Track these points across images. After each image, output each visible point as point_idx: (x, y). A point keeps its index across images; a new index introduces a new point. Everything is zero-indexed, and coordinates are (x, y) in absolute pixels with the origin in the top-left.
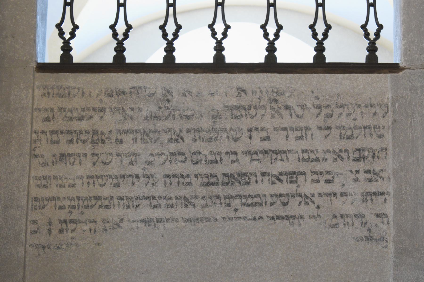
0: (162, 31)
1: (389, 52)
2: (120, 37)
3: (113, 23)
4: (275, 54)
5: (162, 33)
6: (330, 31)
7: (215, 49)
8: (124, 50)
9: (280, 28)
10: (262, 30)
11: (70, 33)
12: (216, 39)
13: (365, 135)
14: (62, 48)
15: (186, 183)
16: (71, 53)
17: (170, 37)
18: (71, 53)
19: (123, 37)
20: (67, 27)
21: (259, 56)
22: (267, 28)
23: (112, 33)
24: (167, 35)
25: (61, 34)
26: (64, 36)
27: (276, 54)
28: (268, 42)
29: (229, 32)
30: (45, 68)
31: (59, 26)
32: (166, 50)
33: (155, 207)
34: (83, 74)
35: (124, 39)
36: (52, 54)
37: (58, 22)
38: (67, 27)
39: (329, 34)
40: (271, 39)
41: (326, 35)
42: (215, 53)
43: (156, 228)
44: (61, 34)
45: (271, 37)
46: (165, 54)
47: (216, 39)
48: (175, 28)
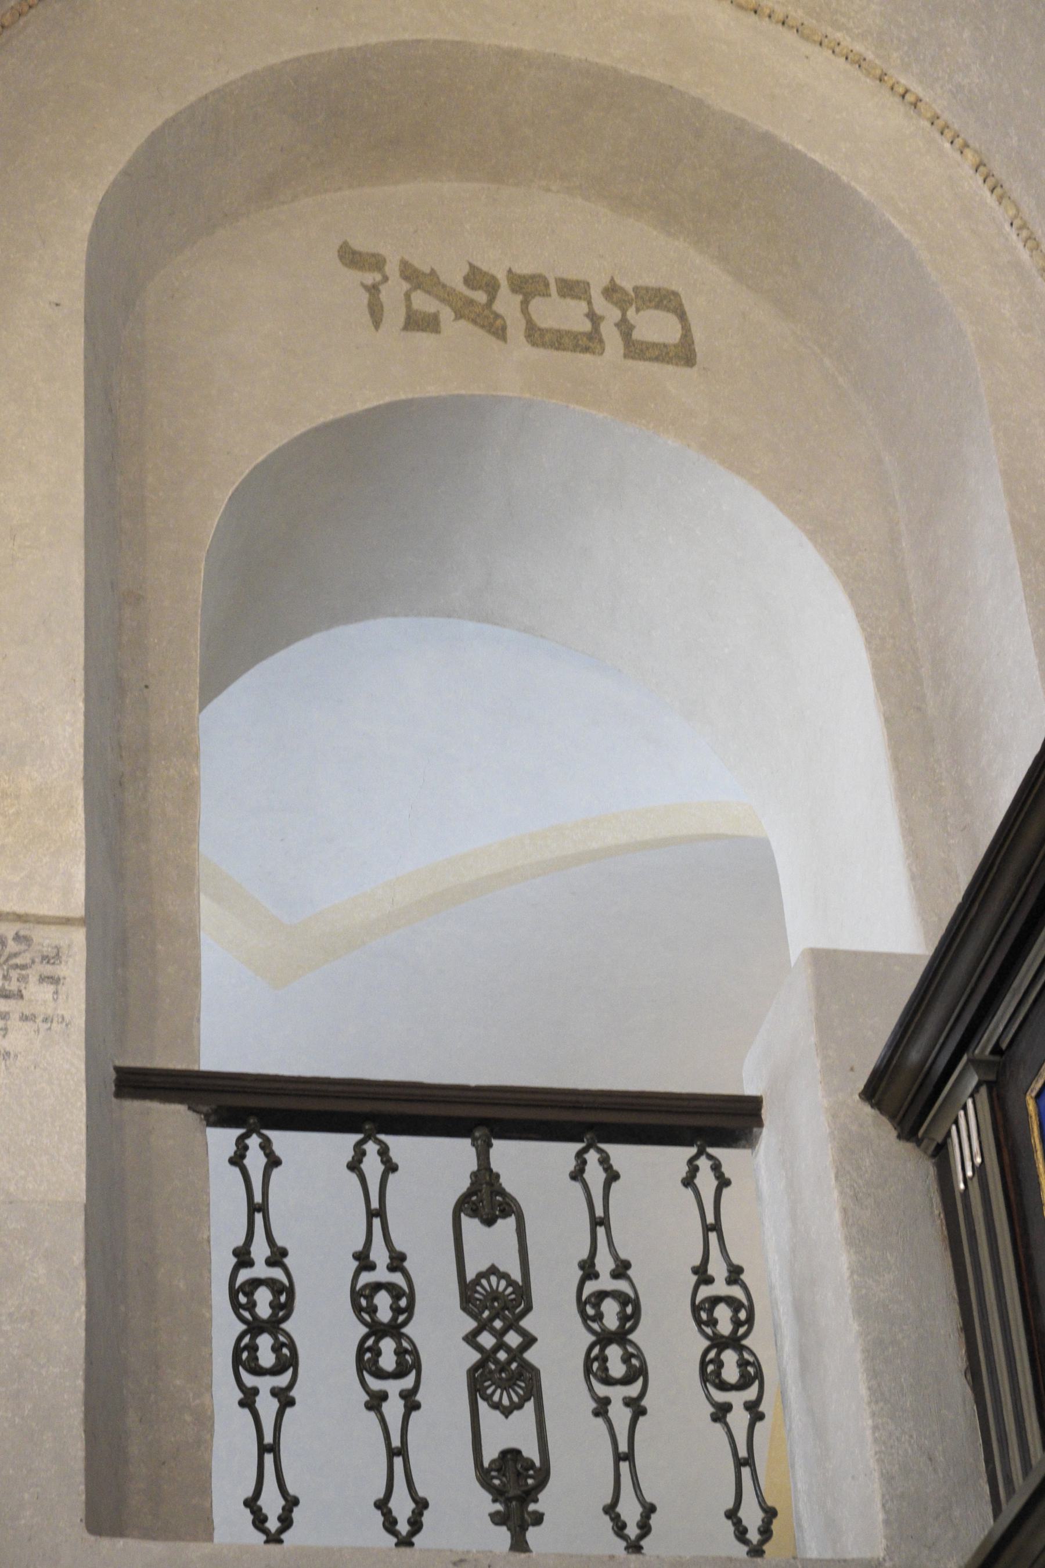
6: (426, 1513)
29: (427, 1518)
40: (633, 1537)
47: (265, 1531)
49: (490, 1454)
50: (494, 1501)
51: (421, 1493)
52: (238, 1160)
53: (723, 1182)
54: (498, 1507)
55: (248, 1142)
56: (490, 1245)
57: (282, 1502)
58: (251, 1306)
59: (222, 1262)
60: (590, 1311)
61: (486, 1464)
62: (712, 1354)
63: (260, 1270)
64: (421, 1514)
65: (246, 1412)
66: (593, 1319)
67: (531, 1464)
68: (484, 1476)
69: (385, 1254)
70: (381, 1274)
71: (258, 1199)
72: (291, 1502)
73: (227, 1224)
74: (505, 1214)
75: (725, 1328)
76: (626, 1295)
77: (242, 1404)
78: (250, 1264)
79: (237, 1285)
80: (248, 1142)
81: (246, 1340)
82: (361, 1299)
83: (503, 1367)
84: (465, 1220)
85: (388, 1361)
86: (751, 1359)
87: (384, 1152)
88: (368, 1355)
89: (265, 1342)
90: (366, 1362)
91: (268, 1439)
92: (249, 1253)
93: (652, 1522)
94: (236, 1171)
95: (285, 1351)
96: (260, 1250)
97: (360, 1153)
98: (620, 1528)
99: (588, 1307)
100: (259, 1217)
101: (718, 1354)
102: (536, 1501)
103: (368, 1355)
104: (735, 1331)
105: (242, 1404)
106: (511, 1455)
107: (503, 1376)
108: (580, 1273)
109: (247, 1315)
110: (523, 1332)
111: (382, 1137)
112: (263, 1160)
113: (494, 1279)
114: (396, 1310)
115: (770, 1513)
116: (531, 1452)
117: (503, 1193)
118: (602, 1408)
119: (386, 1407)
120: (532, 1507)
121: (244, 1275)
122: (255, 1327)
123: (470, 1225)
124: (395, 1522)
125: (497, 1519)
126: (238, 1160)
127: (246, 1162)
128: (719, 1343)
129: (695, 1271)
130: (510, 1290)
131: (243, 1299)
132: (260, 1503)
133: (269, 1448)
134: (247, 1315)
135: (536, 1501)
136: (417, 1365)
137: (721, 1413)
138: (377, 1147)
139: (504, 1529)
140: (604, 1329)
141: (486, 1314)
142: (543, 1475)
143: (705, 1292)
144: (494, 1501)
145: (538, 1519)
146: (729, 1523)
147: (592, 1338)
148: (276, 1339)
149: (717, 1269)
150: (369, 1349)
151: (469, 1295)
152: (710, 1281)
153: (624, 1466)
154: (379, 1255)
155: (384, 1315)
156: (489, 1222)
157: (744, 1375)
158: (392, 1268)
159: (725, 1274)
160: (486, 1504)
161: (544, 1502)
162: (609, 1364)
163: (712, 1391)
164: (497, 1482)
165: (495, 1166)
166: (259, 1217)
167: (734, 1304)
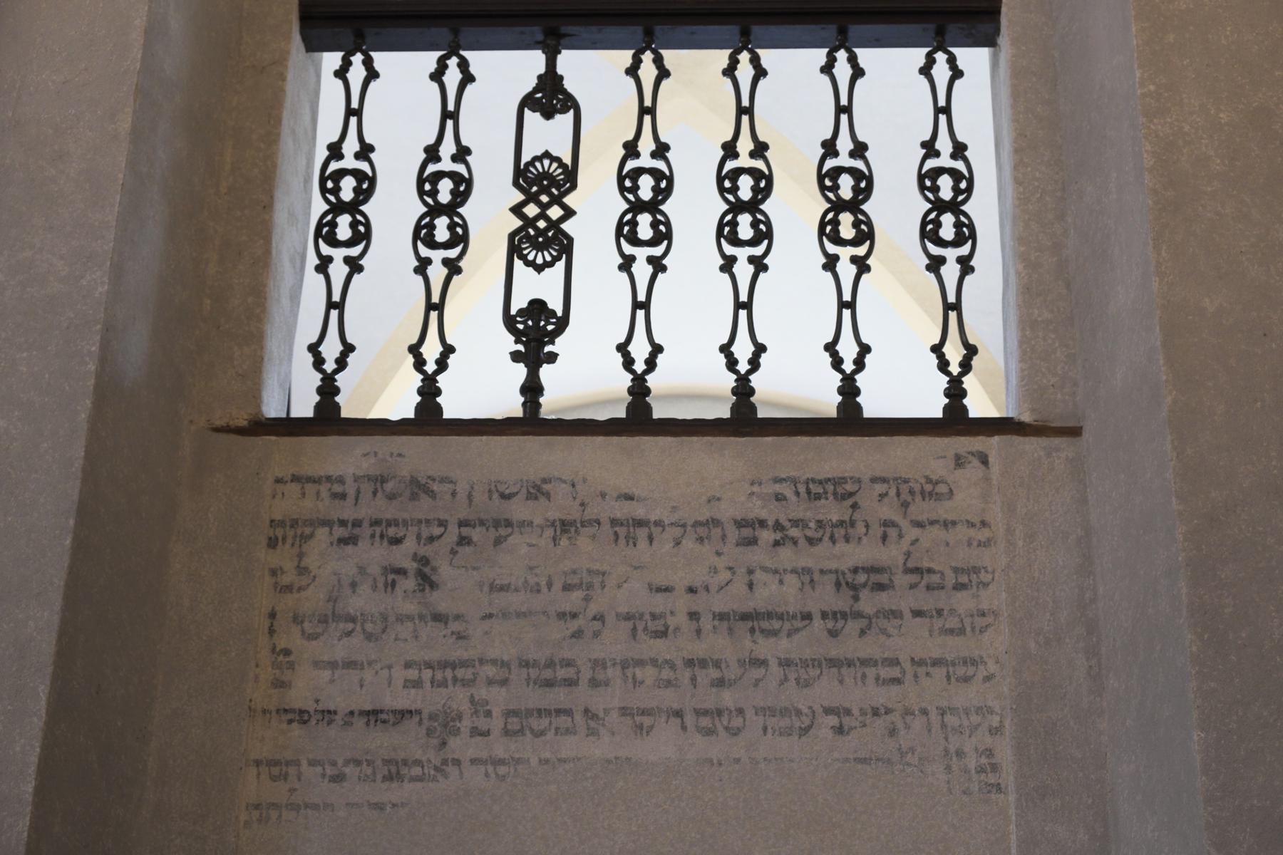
4: (965, 401)
7: (320, 391)
10: (934, 356)
11: (750, 362)
12: (632, 372)
13: (373, 536)
14: (841, 391)
16: (337, 399)
18: (337, 399)
19: (435, 367)
20: (331, 349)
21: (933, 406)
22: (732, 349)
23: (312, 359)
25: (319, 362)
26: (324, 367)
28: (735, 377)
29: (452, 360)
30: (289, 426)
31: (314, 349)
34: (364, 438)
35: (437, 372)
37: (314, 339)
38: (331, 349)
40: (848, 372)
42: (317, 398)
44: (319, 362)
45: (848, 367)
46: (419, 399)
48: (650, 349)
49: (519, 302)
50: (516, 342)
51: (350, 340)
52: (341, 73)
53: (467, 78)
54: (521, 348)
55: (352, 58)
56: (548, 135)
58: (835, 188)
59: (321, 154)
60: (828, 183)
61: (513, 312)
62: (933, 216)
63: (844, 160)
64: (971, 359)
66: (729, 191)
67: (553, 313)
68: (509, 321)
70: (945, 161)
71: (451, 107)
72: (865, 349)
73: (329, 125)
74: (564, 110)
75: (946, 194)
76: (861, 172)
78: (836, 154)
79: (328, 173)
82: (927, 181)
83: (540, 232)
84: (527, 112)
85: (947, 232)
86: (966, 221)
87: (952, 61)
88: (930, 226)
89: (344, 221)
90: (929, 232)
93: (866, 360)
94: (435, 86)
96: (844, 144)
97: (831, 61)
99: (627, 181)
100: (450, 123)
101: (938, 216)
102: (553, 343)
104: (955, 197)
105: (416, 271)
106: (537, 307)
107: (541, 240)
110: (564, 207)
111: (462, 53)
112: (655, 72)
113: (546, 162)
114: (957, 190)
116: (556, 305)
117: (565, 92)
118: (627, 264)
120: (548, 349)
121: (631, 165)
122: (338, 208)
123: (532, 118)
124: (736, 362)
125: (516, 357)
126: (341, 73)
127: (445, 78)
128: (940, 206)
129: (924, 145)
130: (560, 171)
131: (828, 183)
132: (732, 349)
133: (335, 305)
134: (831, 195)
135: (553, 343)
136: (973, 236)
137: (935, 264)
138: (946, 56)
139: (522, 365)
140: (939, 200)
141: (535, 189)
142: (563, 323)
143: (931, 164)
144: (516, 342)
145: (552, 358)
147: (626, 206)
148: (754, 217)
149: (944, 145)
151: (522, 175)
152: (937, 154)
153: (743, 314)
154: (944, 145)
155: (946, 194)
156: (548, 115)
157: (959, 234)
158: (954, 156)
160: (509, 343)
161: (559, 346)
162: (739, 229)
163: (930, 246)
164: (521, 327)
165: (560, 71)
167: (955, 175)
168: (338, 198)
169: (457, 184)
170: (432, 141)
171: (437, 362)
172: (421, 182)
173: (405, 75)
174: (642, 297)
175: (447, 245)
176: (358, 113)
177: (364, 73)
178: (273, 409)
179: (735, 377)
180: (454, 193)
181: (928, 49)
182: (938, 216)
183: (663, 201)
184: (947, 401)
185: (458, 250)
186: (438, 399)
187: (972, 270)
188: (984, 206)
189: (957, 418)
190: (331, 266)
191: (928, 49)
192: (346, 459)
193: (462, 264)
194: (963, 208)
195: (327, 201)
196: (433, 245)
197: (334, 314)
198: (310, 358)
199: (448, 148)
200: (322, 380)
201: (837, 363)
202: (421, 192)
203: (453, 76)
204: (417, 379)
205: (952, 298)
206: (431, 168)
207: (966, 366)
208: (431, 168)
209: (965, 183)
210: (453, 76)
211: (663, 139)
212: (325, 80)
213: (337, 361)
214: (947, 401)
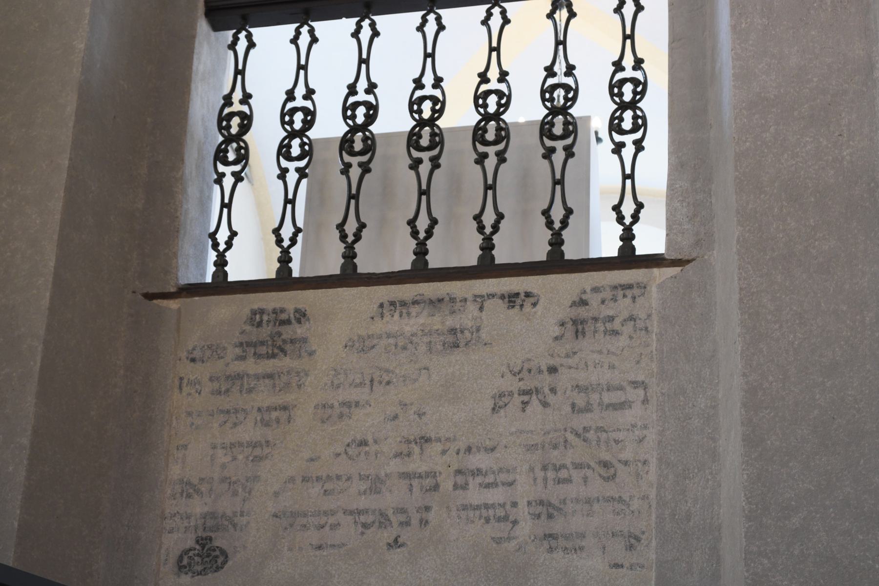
0: (546, 218)
1: (650, 239)
2: (488, 230)
3: (546, 207)
4: (563, 248)
5: (616, 216)
6: (571, 217)
8: (633, 237)
9: (434, 222)
12: (281, 247)
15: (256, 457)
17: (422, 235)
24: (623, 218)
27: (634, 242)
28: (551, 232)
29: (236, 241)
32: (279, 260)
33: (488, 486)
35: (632, 224)
36: (606, 242)
39: (570, 221)
41: (496, 228)
43: (360, 529)
47: (281, 247)
51: (234, 229)
53: (376, 34)
57: (229, 234)
64: (639, 212)
65: (281, 182)
69: (564, 64)
71: (364, 56)
77: (279, 177)
80: (492, 11)
81: (618, 114)
88: (616, 121)
89: (628, 115)
91: (290, 196)
92: (231, 98)
94: (354, 40)
95: (369, 142)
98: (279, 241)
100: (364, 66)
103: (616, 121)
105: (279, 177)
108: (285, 97)
109: (617, 99)
115: (569, 212)
118: (347, 167)
119: (554, 157)
127: (237, 48)
146: (475, 222)
150: (617, 118)
157: (565, 129)
159: (564, 70)
166: (364, 66)
168: (292, 128)
169: (368, 109)
170: (352, 81)
171: (226, 243)
172: (345, 109)
173: (273, 41)
174: (628, 171)
175: (362, 153)
176: (305, 68)
177: (309, 39)
178: (188, 277)
179: (551, 232)
180: (304, 121)
181: (358, 19)
182: (552, 119)
183: (571, 106)
184: (621, 243)
185: (369, 155)
186: (290, 265)
187: (643, 148)
188: (656, 106)
189: (627, 257)
190: (421, 166)
191: (358, 19)
192: (224, 309)
193: (371, 166)
194: (569, 111)
195: (223, 135)
196: (289, 158)
197: (628, 182)
198: (543, 220)
199: (300, 91)
200: (281, 252)
201: (279, 241)
202: (345, 117)
203: (366, 33)
204: (413, 243)
205: (628, 171)
206: (351, 100)
207: (293, 241)
208: (351, 100)
209: (641, 87)
210: (366, 33)
211: (373, 80)
212: (211, 50)
213: (633, 216)
214: (621, 243)
